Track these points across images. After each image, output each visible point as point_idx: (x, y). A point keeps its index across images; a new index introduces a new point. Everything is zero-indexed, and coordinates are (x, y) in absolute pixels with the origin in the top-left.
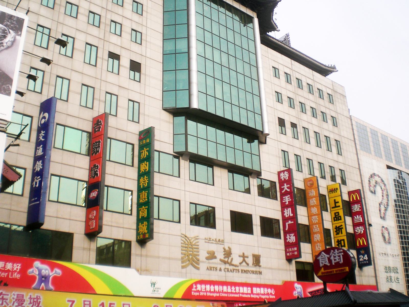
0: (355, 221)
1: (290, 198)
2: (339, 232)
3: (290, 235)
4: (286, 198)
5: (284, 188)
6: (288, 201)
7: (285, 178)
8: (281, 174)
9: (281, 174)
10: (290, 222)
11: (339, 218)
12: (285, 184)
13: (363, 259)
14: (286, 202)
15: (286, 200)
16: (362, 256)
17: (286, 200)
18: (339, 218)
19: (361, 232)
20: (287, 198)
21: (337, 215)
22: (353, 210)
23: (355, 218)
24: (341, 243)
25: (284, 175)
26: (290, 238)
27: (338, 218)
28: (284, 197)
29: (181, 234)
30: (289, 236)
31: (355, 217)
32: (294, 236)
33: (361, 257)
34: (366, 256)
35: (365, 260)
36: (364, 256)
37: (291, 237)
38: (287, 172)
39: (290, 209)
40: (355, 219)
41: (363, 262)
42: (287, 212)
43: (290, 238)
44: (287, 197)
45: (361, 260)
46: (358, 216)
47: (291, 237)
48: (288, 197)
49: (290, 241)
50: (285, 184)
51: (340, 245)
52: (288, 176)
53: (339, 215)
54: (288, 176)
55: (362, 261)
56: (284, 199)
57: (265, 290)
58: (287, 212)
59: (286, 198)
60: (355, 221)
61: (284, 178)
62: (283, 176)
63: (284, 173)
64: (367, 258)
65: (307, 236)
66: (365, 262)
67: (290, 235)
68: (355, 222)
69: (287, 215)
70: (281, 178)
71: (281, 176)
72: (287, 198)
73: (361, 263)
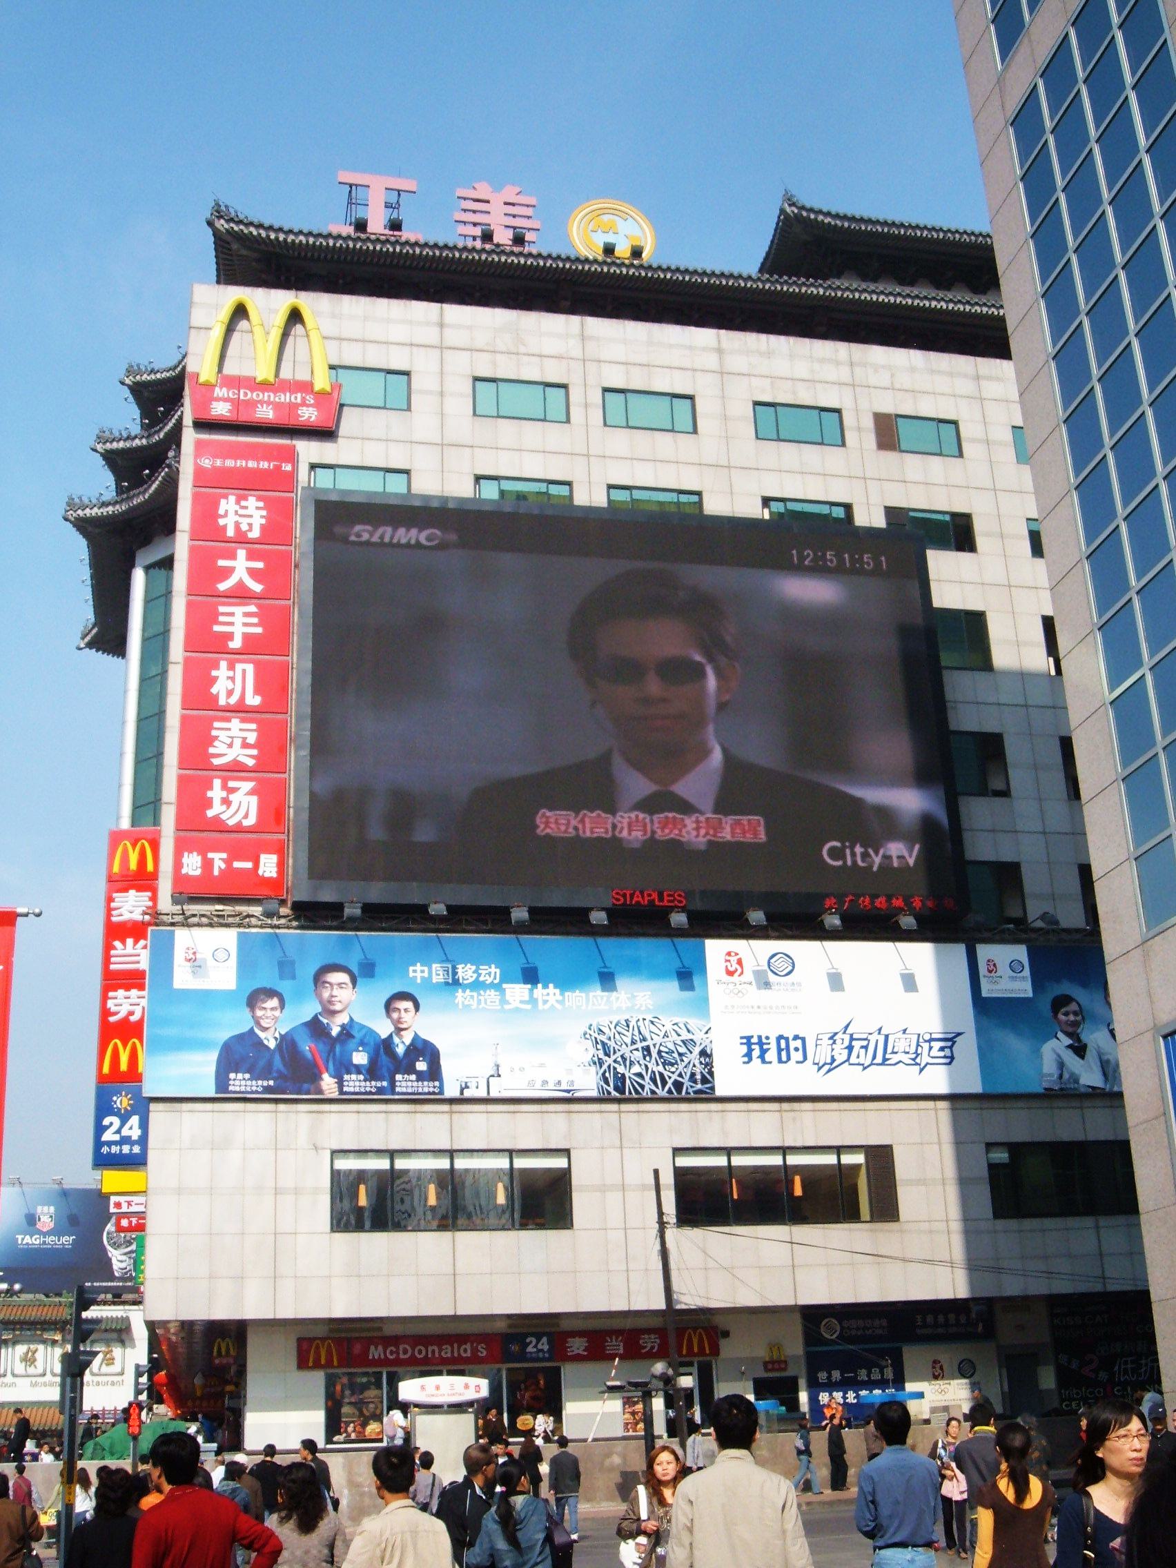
1: (255, 620)
3: (231, 784)
4: (232, 614)
7: (244, 527)
9: (223, 502)
12: (241, 553)
13: (118, 1131)
14: (230, 636)
15: (231, 624)
16: (116, 1121)
17: (231, 624)
23: (115, 948)
25: (241, 512)
26: (226, 802)
28: (222, 609)
29: (506, 204)
32: (252, 792)
33: (111, 1124)
34: (135, 1120)
35: (126, 1140)
36: (124, 1119)
38: (261, 504)
41: (115, 1149)
42: (232, 679)
43: (226, 802)
44: (239, 610)
45: (108, 1136)
48: (247, 615)
49: (224, 817)
50: (241, 553)
52: (263, 521)
55: (109, 1144)
56: (221, 619)
57: (110, 1004)
58: (232, 679)
59: (232, 614)
61: (237, 525)
63: (243, 503)
64: (136, 1134)
66: (126, 1149)
67: (231, 784)
69: (230, 693)
70: (221, 522)
71: (221, 512)
73: (105, 1150)
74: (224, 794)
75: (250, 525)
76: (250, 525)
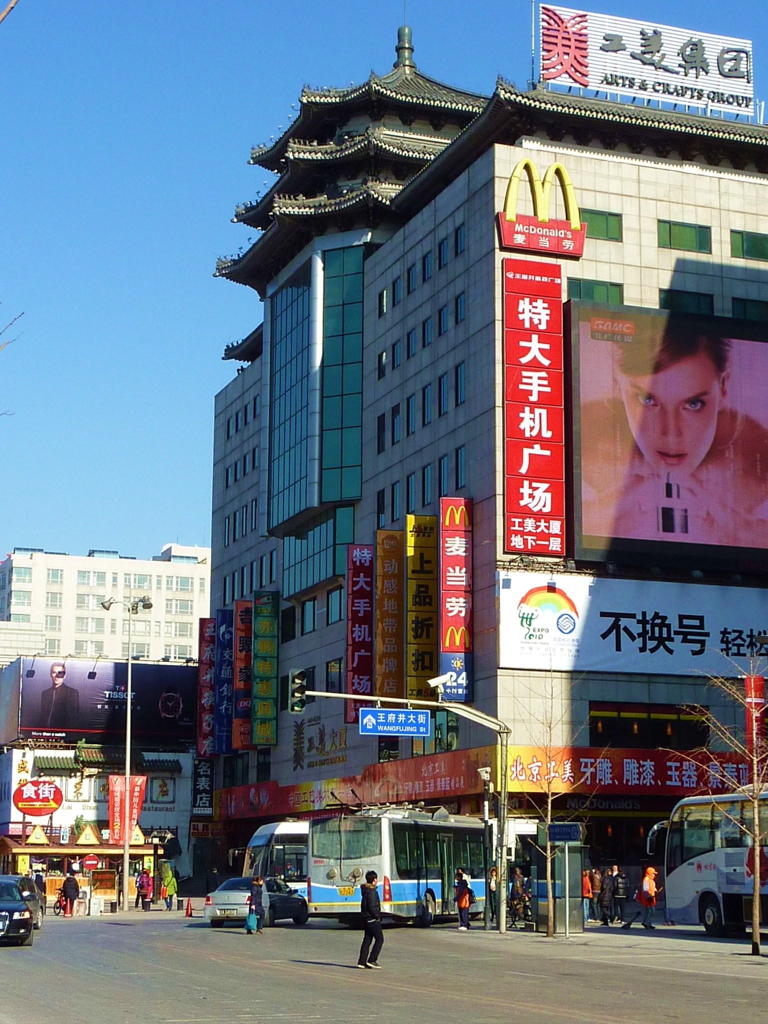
0: (449, 579)
1: (546, 382)
2: (422, 633)
3: (534, 485)
5: (528, 349)
6: (539, 392)
7: (536, 322)
8: (521, 302)
9: (521, 302)
10: (537, 450)
11: (427, 600)
13: (456, 681)
14: (530, 393)
18: (427, 600)
19: (460, 612)
20: (535, 381)
21: (422, 592)
22: (448, 550)
24: (423, 660)
25: (534, 310)
26: (531, 496)
27: (425, 600)
30: (530, 487)
31: (450, 569)
37: (535, 493)
38: (546, 305)
39: (544, 412)
40: (448, 574)
46: (457, 568)
47: (535, 493)
48: (540, 378)
49: (530, 506)
51: (420, 663)
53: (427, 591)
54: (548, 318)
56: (524, 380)
59: (531, 378)
60: (449, 579)
61: (531, 319)
62: (527, 311)
63: (534, 304)
65: (699, 681)
68: (448, 583)
69: (532, 429)
70: (521, 317)
71: (520, 310)
72: (535, 381)
74: (531, 491)
75: (540, 320)
76: (540, 320)
